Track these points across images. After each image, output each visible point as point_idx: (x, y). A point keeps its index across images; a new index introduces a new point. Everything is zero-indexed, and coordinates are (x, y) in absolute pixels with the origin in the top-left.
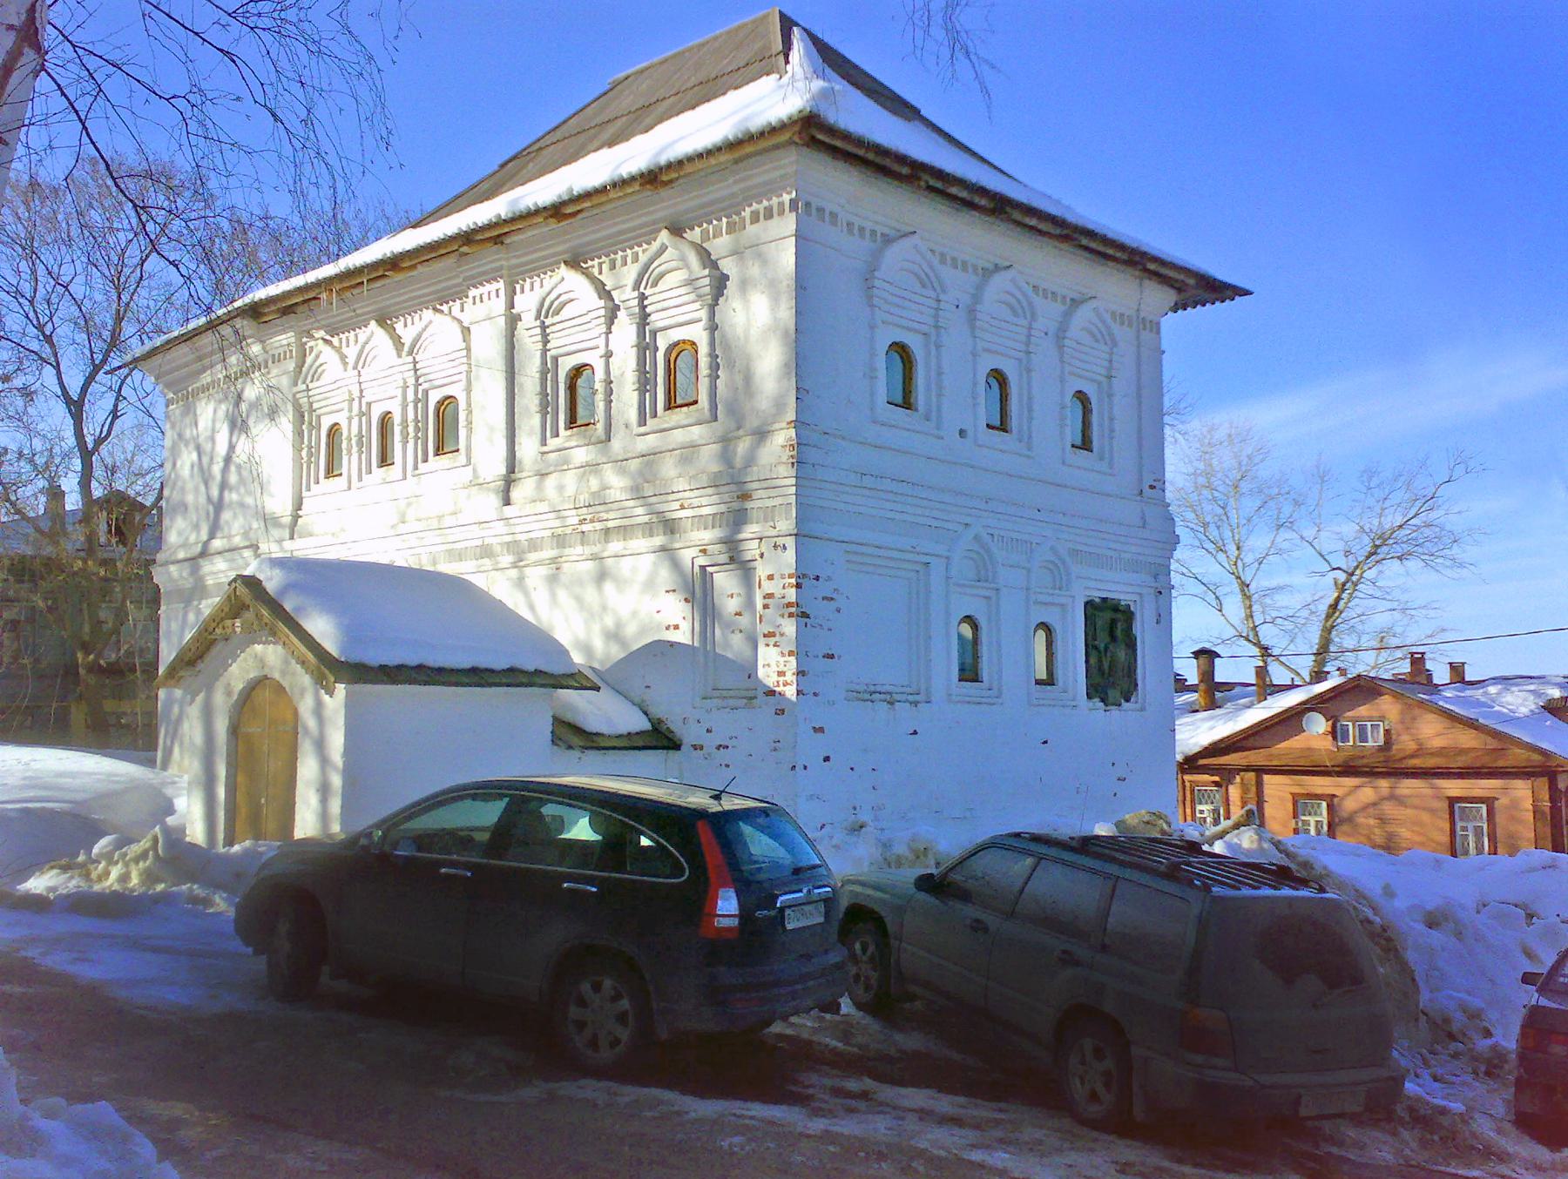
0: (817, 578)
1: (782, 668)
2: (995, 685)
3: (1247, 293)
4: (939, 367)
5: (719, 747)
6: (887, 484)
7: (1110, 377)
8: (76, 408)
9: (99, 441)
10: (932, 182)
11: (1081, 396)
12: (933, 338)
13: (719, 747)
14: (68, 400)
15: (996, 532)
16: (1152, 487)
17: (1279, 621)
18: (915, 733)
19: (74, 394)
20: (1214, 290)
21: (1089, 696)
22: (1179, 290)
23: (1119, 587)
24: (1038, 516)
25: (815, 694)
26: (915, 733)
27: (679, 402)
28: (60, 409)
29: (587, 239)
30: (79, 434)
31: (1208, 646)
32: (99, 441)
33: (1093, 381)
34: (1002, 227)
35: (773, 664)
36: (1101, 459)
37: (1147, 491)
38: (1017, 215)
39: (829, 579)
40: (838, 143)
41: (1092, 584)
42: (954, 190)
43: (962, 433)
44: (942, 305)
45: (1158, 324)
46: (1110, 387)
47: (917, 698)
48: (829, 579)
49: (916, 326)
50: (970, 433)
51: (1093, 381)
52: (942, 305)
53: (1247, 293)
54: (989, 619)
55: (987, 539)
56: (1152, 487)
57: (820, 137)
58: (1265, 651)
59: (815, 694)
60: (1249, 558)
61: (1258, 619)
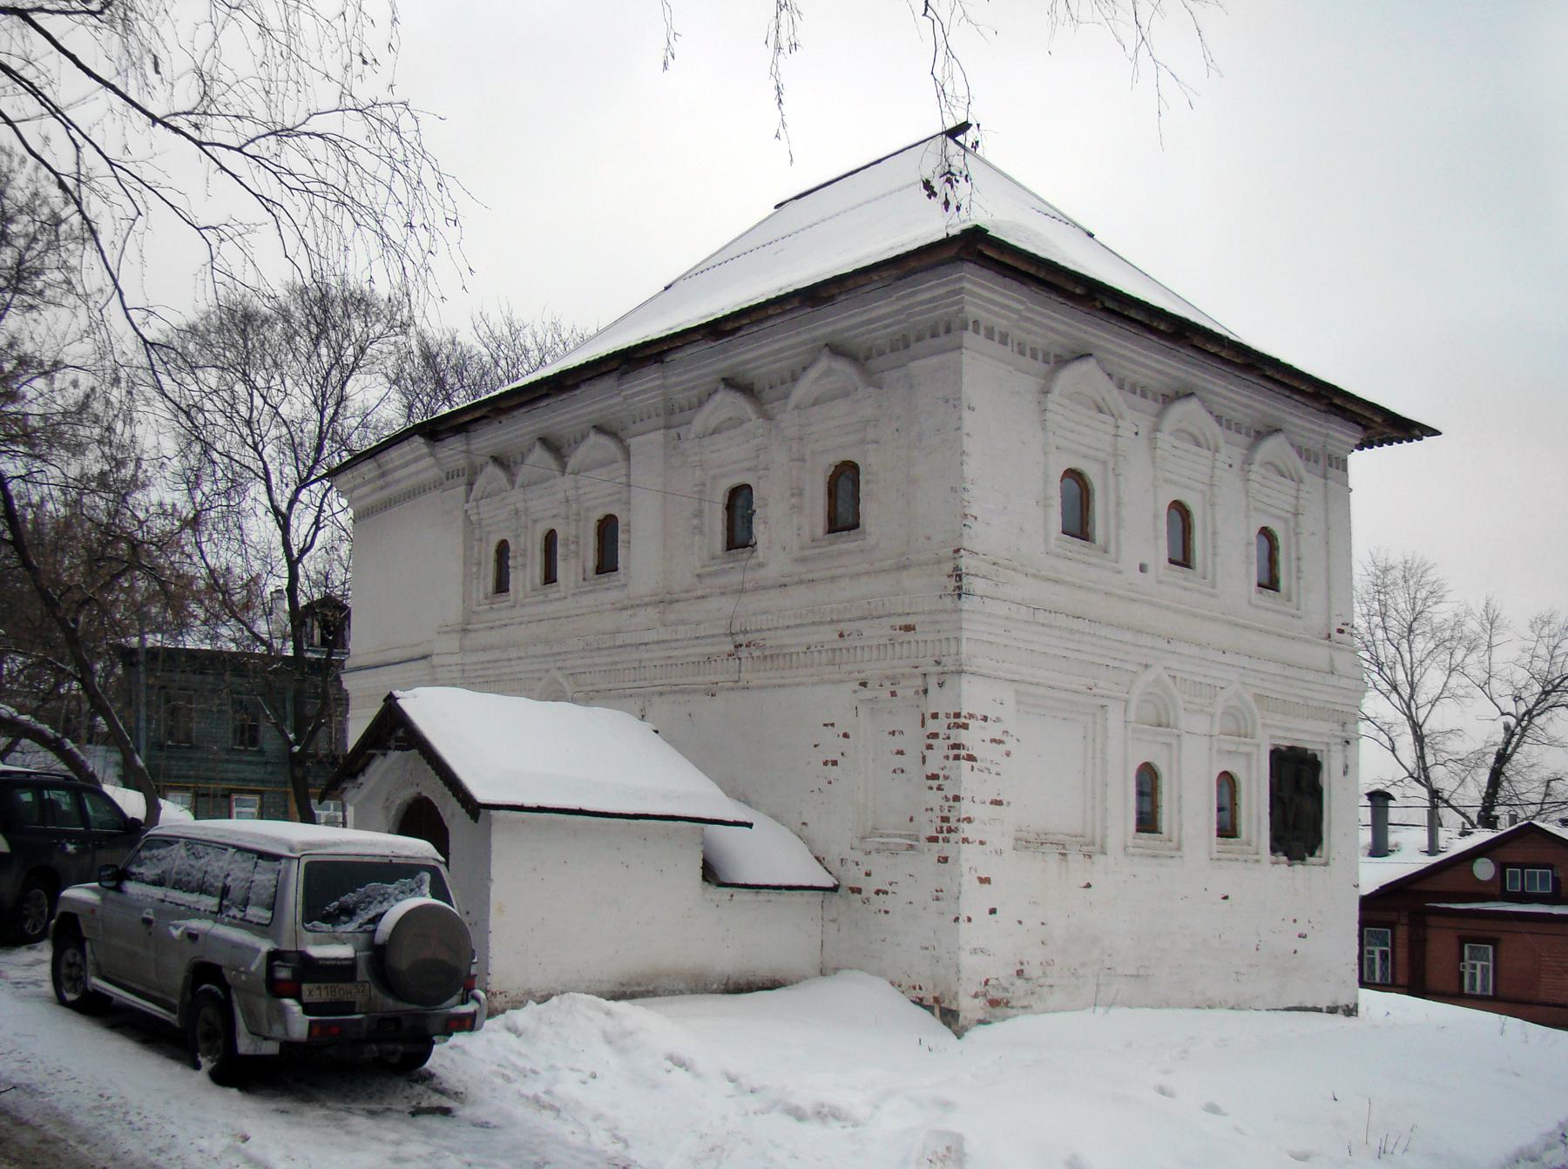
0: (985, 719)
1: (946, 814)
2: (1175, 837)
3: (1436, 433)
4: (1118, 497)
5: (877, 892)
6: (1062, 620)
7: (1296, 514)
8: (284, 521)
9: (303, 552)
10: (1109, 304)
11: (1266, 532)
12: (1111, 466)
13: (877, 892)
14: (276, 511)
15: (1178, 675)
16: (1341, 631)
17: (1450, 764)
18: (1089, 886)
19: (283, 507)
20: (1401, 429)
21: (1273, 850)
22: (1366, 428)
23: (1304, 734)
24: (1223, 658)
25: (982, 843)
26: (1089, 886)
27: (839, 525)
28: (270, 523)
29: (746, 357)
30: (286, 544)
31: (1381, 787)
32: (303, 552)
33: (1279, 518)
34: (1185, 352)
35: (937, 809)
36: (1289, 600)
37: (1335, 635)
38: (1197, 341)
39: (998, 720)
40: (1009, 261)
41: (1280, 733)
42: (1132, 313)
43: (1143, 568)
44: (1121, 431)
45: (1345, 461)
46: (1297, 525)
47: (1091, 848)
48: (998, 720)
49: (1092, 452)
50: (1151, 569)
51: (1279, 518)
52: (1121, 431)
53: (1436, 433)
54: (1170, 769)
55: (1169, 681)
56: (1341, 631)
57: (988, 253)
58: (1435, 794)
59: (982, 843)
60: (1421, 698)
61: (1429, 760)
